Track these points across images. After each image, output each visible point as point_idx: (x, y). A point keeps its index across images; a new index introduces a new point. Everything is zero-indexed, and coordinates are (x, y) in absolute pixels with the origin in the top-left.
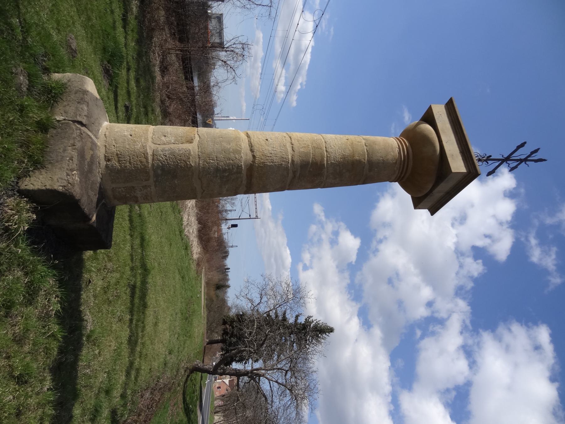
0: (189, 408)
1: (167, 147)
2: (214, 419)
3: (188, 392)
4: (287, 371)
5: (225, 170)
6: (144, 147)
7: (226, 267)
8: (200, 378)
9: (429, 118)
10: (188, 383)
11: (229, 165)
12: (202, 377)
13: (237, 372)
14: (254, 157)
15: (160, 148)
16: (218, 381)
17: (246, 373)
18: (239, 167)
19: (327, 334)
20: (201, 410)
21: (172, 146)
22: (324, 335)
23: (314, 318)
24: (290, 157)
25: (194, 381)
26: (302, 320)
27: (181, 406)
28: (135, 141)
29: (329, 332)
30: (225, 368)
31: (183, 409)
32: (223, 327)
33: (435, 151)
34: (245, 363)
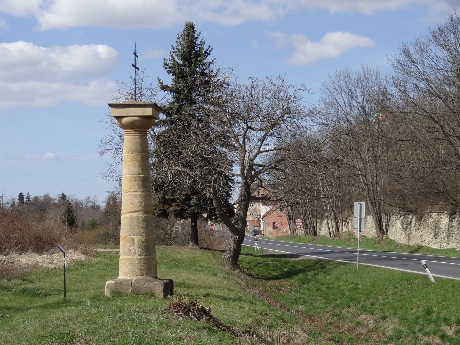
0: (287, 272)
1: (137, 250)
2: (324, 236)
3: (266, 274)
4: (249, 127)
5: (147, 224)
6: (137, 260)
7: (17, 201)
8: (249, 257)
9: (119, 118)
10: (253, 273)
11: (144, 222)
12: (247, 254)
13: (244, 200)
14: (140, 210)
15: (137, 253)
16: (262, 228)
17: (247, 187)
18: (145, 217)
19: (196, 35)
20: (297, 256)
21: (136, 247)
22: (198, 42)
23: (168, 57)
24: (140, 193)
25: (251, 265)
26: (169, 80)
27: (282, 281)
28: (134, 264)
29: (194, 32)
30: (236, 216)
31: (287, 279)
32: (171, 216)
33: (139, 120)
34: (233, 182)
